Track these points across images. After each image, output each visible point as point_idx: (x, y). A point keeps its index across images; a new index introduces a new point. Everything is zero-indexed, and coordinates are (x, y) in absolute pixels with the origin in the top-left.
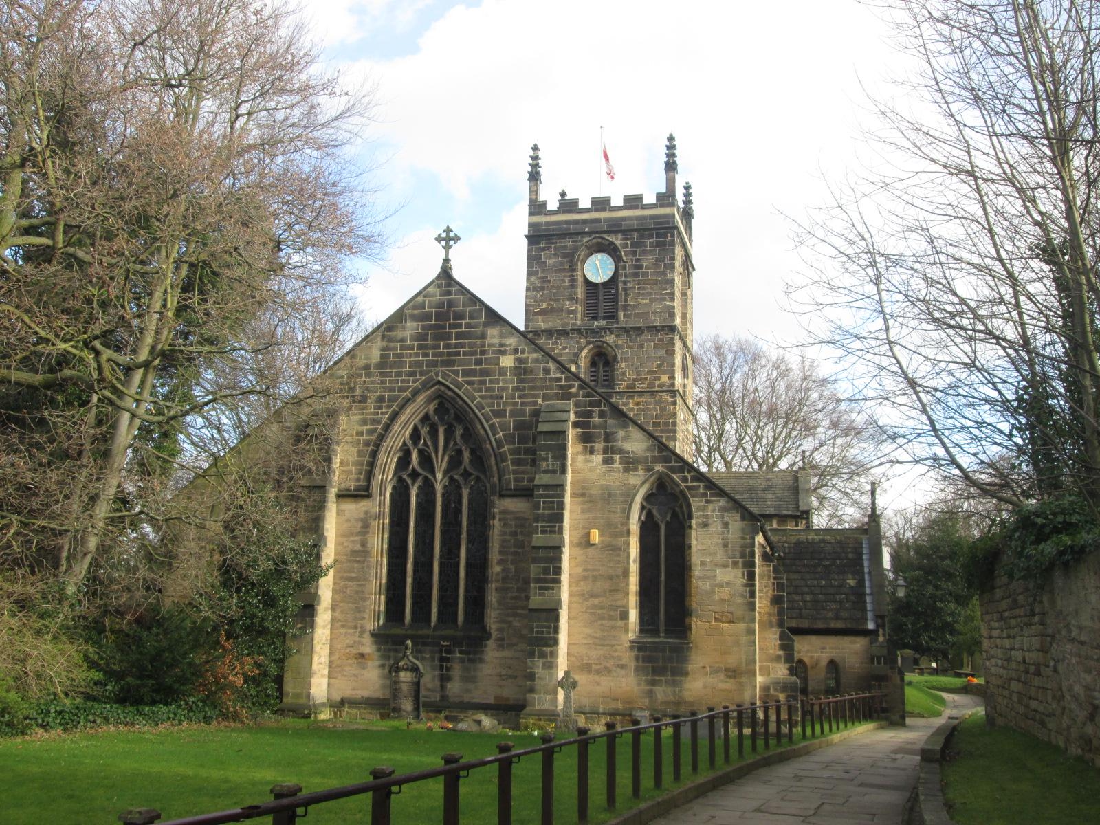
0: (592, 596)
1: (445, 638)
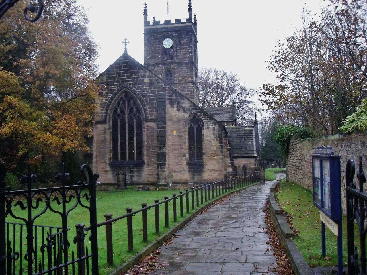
1: (131, 165)
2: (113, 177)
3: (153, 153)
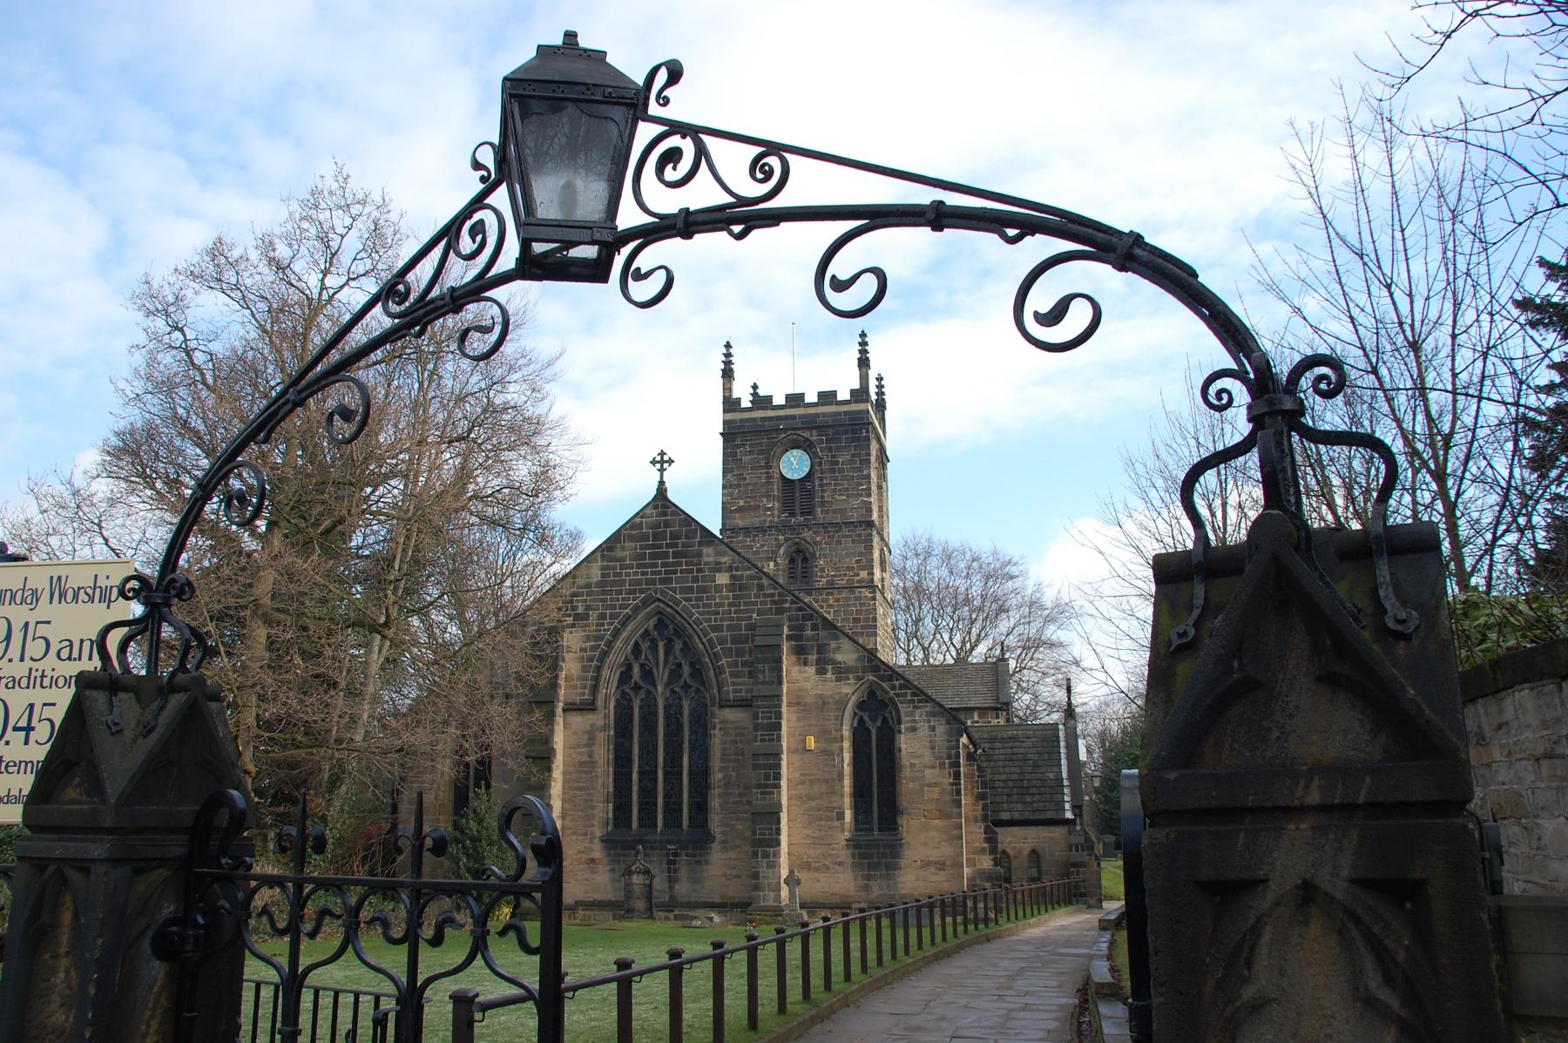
1: (671, 843)
2: (613, 880)
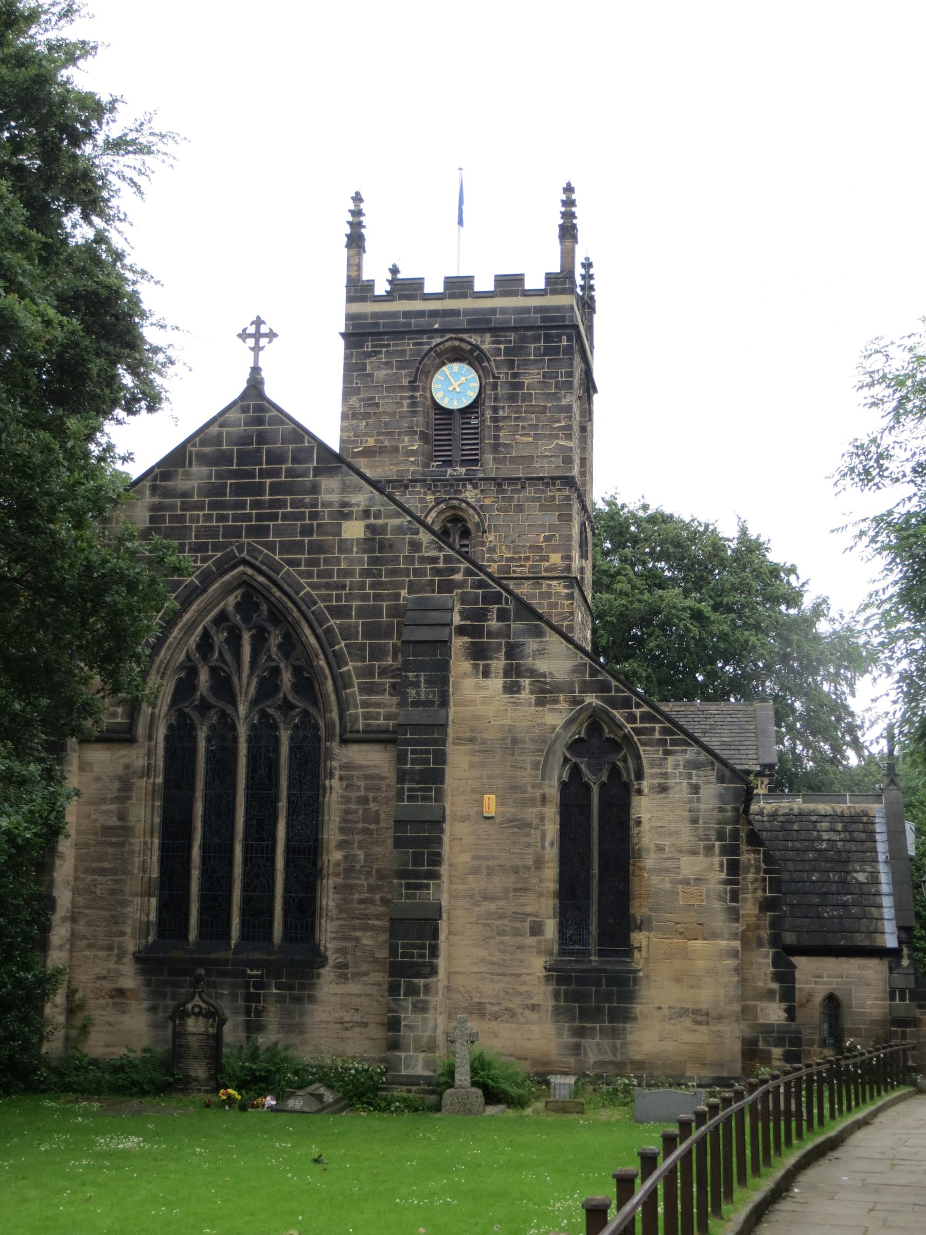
0: (486, 898)
1: (254, 965)
2: (154, 1026)
3: (372, 910)
